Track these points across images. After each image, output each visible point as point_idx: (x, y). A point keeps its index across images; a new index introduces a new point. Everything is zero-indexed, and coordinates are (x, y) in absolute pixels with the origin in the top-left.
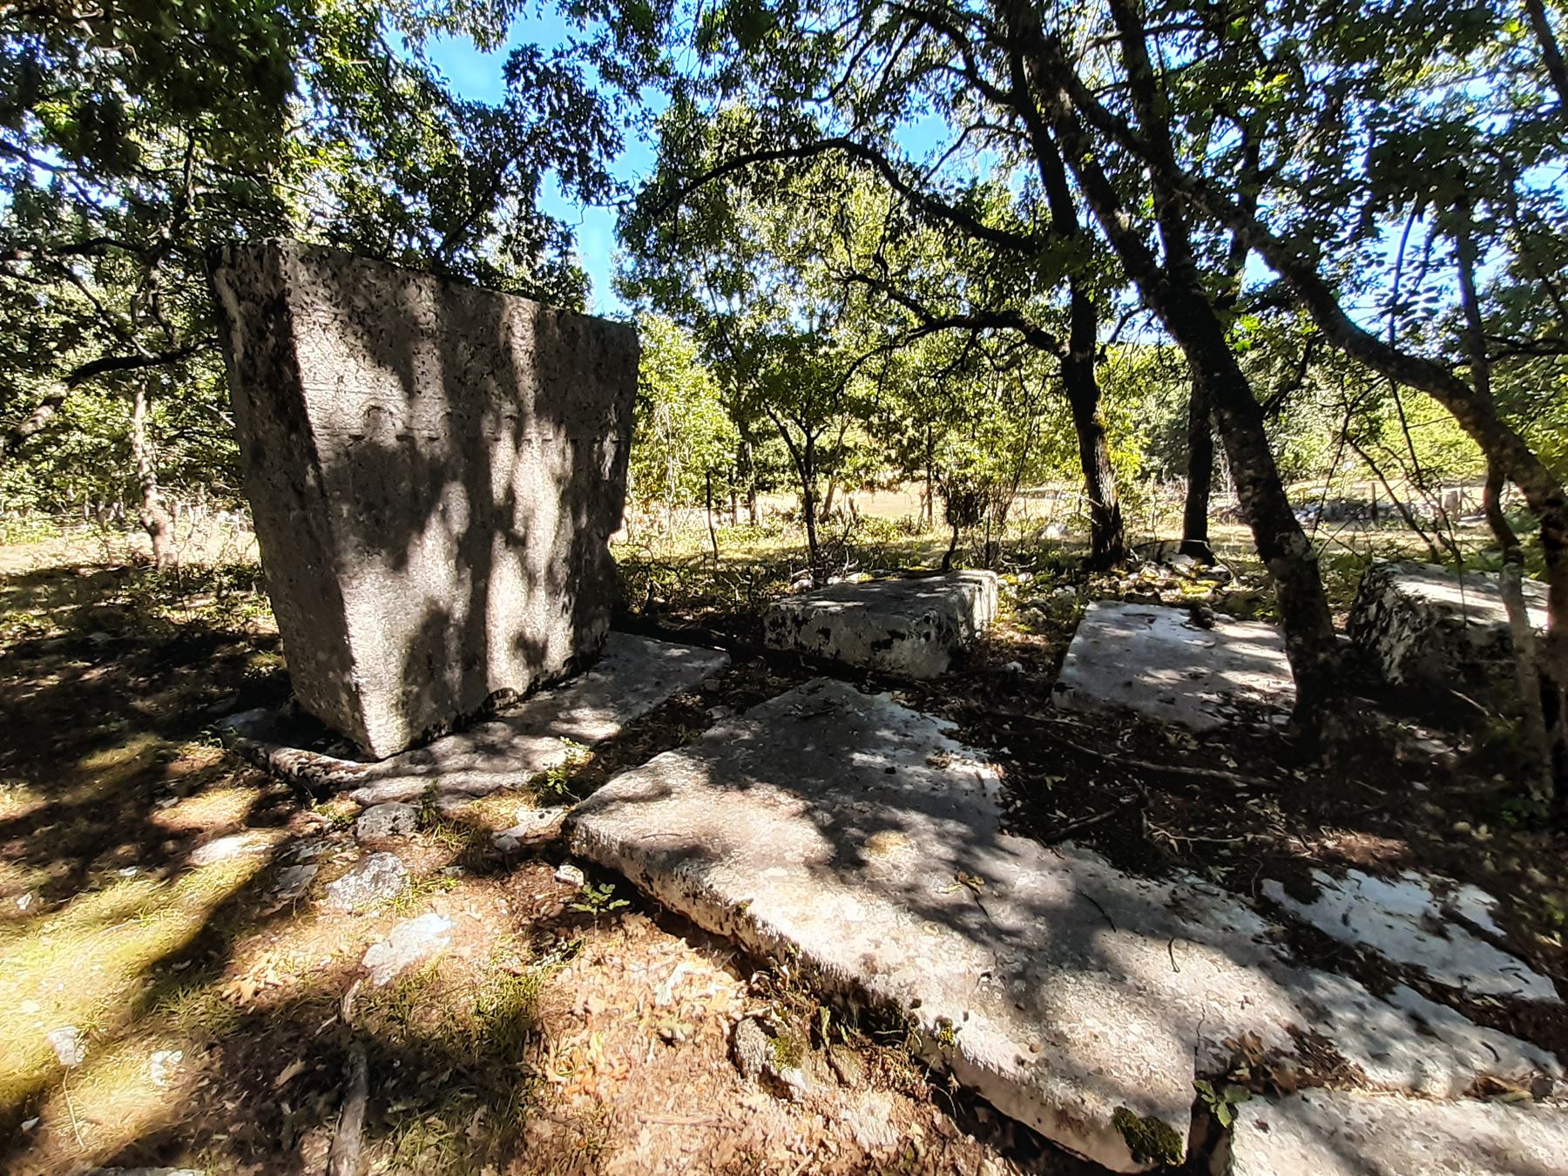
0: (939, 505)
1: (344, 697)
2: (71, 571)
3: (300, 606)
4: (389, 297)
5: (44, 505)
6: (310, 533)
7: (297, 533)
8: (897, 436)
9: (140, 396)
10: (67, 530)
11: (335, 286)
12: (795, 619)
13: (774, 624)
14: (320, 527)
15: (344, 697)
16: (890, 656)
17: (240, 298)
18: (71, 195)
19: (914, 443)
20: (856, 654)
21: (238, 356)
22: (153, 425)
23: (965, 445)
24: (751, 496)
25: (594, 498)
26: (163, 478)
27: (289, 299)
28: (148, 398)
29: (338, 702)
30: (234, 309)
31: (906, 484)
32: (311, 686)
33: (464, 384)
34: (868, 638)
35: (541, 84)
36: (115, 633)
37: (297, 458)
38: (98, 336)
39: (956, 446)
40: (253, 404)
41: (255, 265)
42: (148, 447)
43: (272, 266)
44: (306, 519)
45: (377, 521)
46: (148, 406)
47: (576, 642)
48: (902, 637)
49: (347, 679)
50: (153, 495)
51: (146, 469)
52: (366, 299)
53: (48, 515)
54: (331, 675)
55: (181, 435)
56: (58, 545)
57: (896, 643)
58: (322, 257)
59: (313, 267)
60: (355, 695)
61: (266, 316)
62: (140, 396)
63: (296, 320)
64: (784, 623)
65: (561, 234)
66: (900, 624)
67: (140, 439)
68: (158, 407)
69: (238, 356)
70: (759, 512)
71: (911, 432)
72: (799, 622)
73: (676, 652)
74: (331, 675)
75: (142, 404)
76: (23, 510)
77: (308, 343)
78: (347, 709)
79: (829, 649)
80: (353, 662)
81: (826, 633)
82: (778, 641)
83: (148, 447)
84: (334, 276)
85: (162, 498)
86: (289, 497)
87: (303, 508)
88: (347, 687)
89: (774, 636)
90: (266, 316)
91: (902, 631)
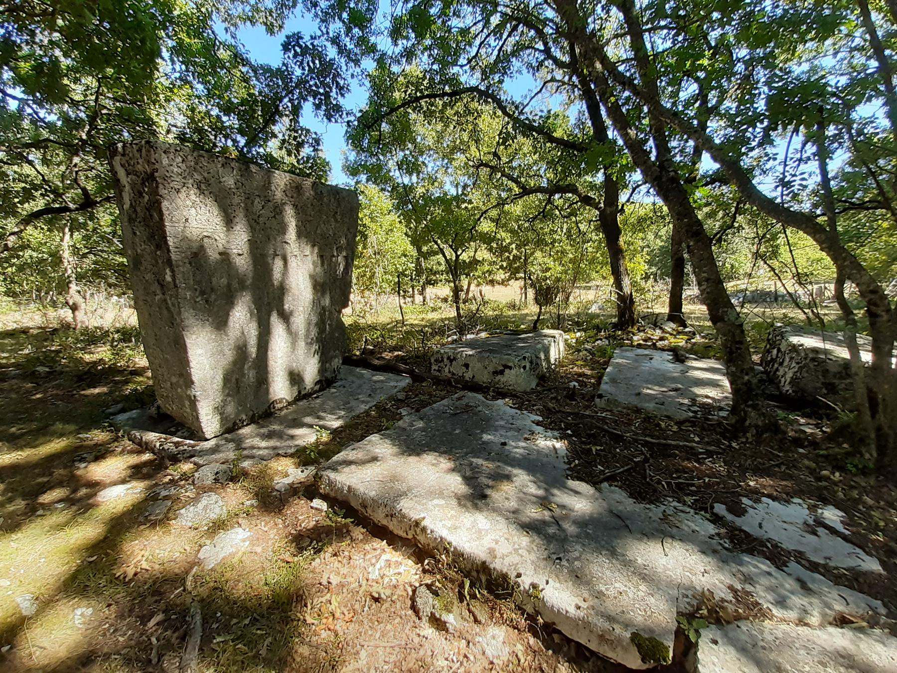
0: (531, 293)
1: (187, 403)
6: (168, 308)
8: (507, 254)
9: (67, 230)
12: (449, 358)
14: (174, 305)
15: (187, 403)
17: (128, 174)
18: (29, 114)
20: (484, 377)
24: (423, 289)
26: (80, 277)
28: (70, 230)
31: (512, 282)
33: (258, 223)
34: (491, 369)
35: (303, 54)
36: (50, 367)
39: (540, 260)
40: (135, 234)
44: (165, 300)
46: (71, 236)
47: (322, 371)
48: (510, 368)
49: (189, 392)
50: (73, 287)
51: (69, 271)
53: (11, 299)
54: (179, 390)
55: (90, 253)
56: (18, 316)
57: (507, 371)
61: (143, 184)
64: (443, 360)
66: (509, 360)
67: (66, 254)
71: (515, 252)
72: (451, 360)
74: (179, 390)
78: (188, 410)
79: (468, 376)
80: (193, 382)
81: (467, 366)
82: (439, 371)
83: (71, 259)
84: (183, 161)
85: (79, 288)
86: (156, 287)
89: (437, 368)
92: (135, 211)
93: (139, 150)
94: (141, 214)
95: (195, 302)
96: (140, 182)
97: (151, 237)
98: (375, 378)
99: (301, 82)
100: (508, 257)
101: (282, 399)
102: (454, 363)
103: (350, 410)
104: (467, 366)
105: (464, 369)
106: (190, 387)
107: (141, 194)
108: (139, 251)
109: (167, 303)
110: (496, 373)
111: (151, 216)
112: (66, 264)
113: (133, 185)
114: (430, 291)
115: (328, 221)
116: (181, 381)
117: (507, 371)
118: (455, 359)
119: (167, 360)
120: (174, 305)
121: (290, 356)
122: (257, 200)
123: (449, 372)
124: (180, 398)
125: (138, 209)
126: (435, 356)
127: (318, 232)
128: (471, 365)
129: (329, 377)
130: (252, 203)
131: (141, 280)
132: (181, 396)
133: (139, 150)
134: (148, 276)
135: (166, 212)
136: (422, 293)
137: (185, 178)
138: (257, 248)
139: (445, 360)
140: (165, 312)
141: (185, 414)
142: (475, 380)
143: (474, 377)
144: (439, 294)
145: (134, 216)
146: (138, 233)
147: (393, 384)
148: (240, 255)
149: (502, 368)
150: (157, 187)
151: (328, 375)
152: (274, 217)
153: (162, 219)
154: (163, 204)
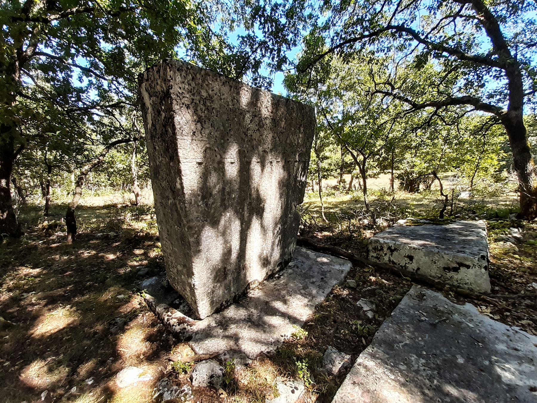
0: (397, 183)
1: (188, 289)
2: (114, 206)
3: (172, 243)
4: (217, 91)
5: (112, 185)
6: (177, 210)
7: (171, 210)
8: (378, 157)
9: (134, 153)
10: (116, 192)
11: (193, 84)
12: (389, 248)
13: (375, 249)
14: (181, 209)
15: (188, 289)
16: (456, 276)
17: (150, 96)
18: (115, 89)
19: (385, 159)
20: (433, 272)
21: (149, 126)
22: (137, 161)
23: (414, 159)
24: (320, 181)
25: (292, 190)
26: (139, 177)
27: (171, 91)
28: (136, 153)
29: (185, 289)
30: (148, 102)
31: (382, 175)
32: (174, 278)
33: (247, 135)
34: (441, 264)
35: (266, 22)
36: (117, 233)
37: (173, 174)
38: (120, 133)
39: (409, 160)
40: (155, 148)
41: (157, 77)
42: (135, 168)
43: (164, 74)
44: (175, 204)
45: (207, 205)
46: (136, 156)
47: (282, 255)
48: (468, 267)
49: (190, 281)
50: (136, 183)
51: (134, 175)
52: (207, 92)
53: (112, 188)
54: (183, 277)
55: (144, 165)
56: (111, 197)
57: (463, 269)
58: (188, 68)
59: (183, 74)
60: (192, 289)
61: (161, 103)
62: (134, 153)
63: (174, 102)
64: (382, 249)
65: (268, 83)
66: (466, 259)
67: (133, 166)
68: (139, 156)
69: (149, 126)
70: (323, 186)
71: (384, 155)
72: (392, 250)
73: (325, 260)
74: (183, 277)
75: (134, 155)
76: (105, 186)
77: (179, 115)
78: (189, 294)
79: (412, 266)
80: (193, 274)
81: (411, 258)
82: (378, 258)
83: (135, 168)
84: (193, 78)
85: (138, 184)
86: (168, 193)
87: (174, 199)
88: (190, 285)
89: (375, 255)
90: (161, 103)
91: (468, 263)
92: (156, 129)
93: (158, 71)
94: (159, 131)
95: (198, 206)
96: (159, 101)
97: (167, 149)
98: (319, 259)
99: (263, 44)
100: (379, 158)
101: (255, 281)
102: (395, 253)
103: (91, 67)
104: (411, 258)
105: (407, 260)
106: (191, 277)
107: (159, 112)
108: (158, 163)
109: (177, 207)
110: (447, 269)
111: (167, 131)
112: (133, 170)
113: (154, 105)
114: (324, 182)
115: (295, 132)
116: (185, 271)
117: (463, 269)
118: (395, 249)
119: (175, 252)
120: (181, 209)
121: (261, 244)
122: (248, 115)
123: (390, 260)
124: (183, 283)
125: (158, 127)
126: (374, 245)
127: (288, 141)
128: (416, 257)
129: (287, 259)
130: (244, 118)
131: (159, 187)
132: (184, 282)
133: (158, 71)
134: (164, 184)
135: (178, 127)
136: (319, 183)
137: (194, 95)
138: (245, 157)
139: (385, 249)
140: (175, 214)
141: (187, 296)
142: (419, 272)
143: (418, 269)
144: (330, 184)
145: (154, 133)
146: (157, 148)
147: (337, 267)
148: (232, 163)
149: (455, 265)
150: (171, 103)
151: (286, 257)
152: (258, 130)
153: (174, 134)
154: (176, 118)
